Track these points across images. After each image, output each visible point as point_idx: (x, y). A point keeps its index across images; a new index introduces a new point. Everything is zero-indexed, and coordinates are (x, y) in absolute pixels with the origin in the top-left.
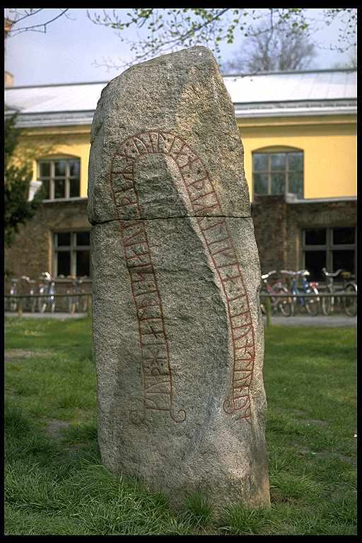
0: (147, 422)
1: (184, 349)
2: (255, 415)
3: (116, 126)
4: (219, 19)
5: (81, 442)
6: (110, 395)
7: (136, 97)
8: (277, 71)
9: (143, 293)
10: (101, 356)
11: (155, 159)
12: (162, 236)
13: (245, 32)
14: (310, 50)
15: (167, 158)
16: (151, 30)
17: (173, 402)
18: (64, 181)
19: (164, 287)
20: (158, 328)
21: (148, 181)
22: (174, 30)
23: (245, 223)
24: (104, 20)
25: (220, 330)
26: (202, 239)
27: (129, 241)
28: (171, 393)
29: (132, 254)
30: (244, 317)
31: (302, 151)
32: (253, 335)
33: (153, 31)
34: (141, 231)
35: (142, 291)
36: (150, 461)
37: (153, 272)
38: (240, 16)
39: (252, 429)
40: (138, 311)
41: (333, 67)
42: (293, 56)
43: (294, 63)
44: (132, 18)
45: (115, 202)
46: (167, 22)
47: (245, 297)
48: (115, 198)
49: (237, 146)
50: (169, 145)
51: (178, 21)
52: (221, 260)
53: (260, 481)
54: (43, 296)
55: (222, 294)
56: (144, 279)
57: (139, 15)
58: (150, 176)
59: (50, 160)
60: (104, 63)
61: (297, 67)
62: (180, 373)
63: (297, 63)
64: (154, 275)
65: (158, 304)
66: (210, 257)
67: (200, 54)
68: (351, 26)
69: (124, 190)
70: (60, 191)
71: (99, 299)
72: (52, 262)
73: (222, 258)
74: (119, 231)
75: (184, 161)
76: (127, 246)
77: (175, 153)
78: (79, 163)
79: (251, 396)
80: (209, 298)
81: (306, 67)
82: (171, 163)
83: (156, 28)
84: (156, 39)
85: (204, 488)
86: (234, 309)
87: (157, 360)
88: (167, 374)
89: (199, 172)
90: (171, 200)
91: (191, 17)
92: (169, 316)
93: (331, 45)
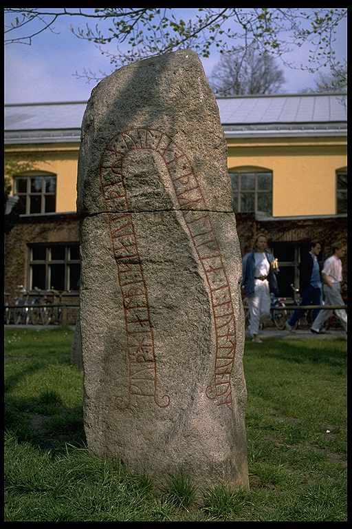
0: (132, 407)
2: (235, 401)
4: (196, 37)
5: (63, 434)
6: (96, 381)
8: (246, 95)
9: (129, 283)
10: (88, 343)
13: (220, 48)
14: (279, 76)
16: (131, 45)
17: (157, 388)
22: (153, 45)
23: (227, 218)
24: (87, 35)
26: (187, 231)
28: (156, 379)
30: (226, 306)
31: (271, 171)
33: (134, 45)
35: (129, 281)
36: (135, 445)
37: (140, 262)
38: (216, 35)
39: (233, 415)
41: (301, 93)
42: (262, 82)
43: (263, 88)
44: (113, 34)
46: (147, 38)
47: (227, 288)
48: (104, 192)
51: (157, 37)
52: (205, 252)
53: (240, 466)
54: (18, 307)
56: (130, 270)
57: (120, 31)
59: (27, 176)
60: (85, 75)
61: (267, 93)
63: (267, 88)
66: (194, 250)
67: (187, 57)
68: (321, 48)
69: (113, 184)
70: (36, 207)
71: (86, 289)
72: (29, 276)
73: (207, 250)
77: (162, 149)
78: (55, 180)
79: (232, 383)
80: (193, 288)
81: (275, 92)
83: (136, 43)
84: (136, 54)
85: (185, 471)
86: (217, 299)
87: (143, 347)
88: (152, 361)
89: (184, 168)
93: (302, 66)
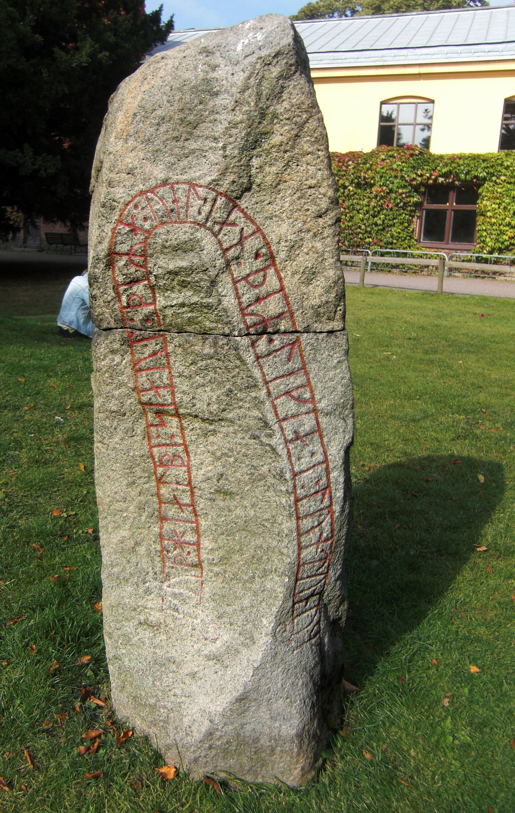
26: (257, 373)
56: (163, 424)
65: (184, 466)
89: (257, 255)
90: (208, 306)
91: (260, 52)
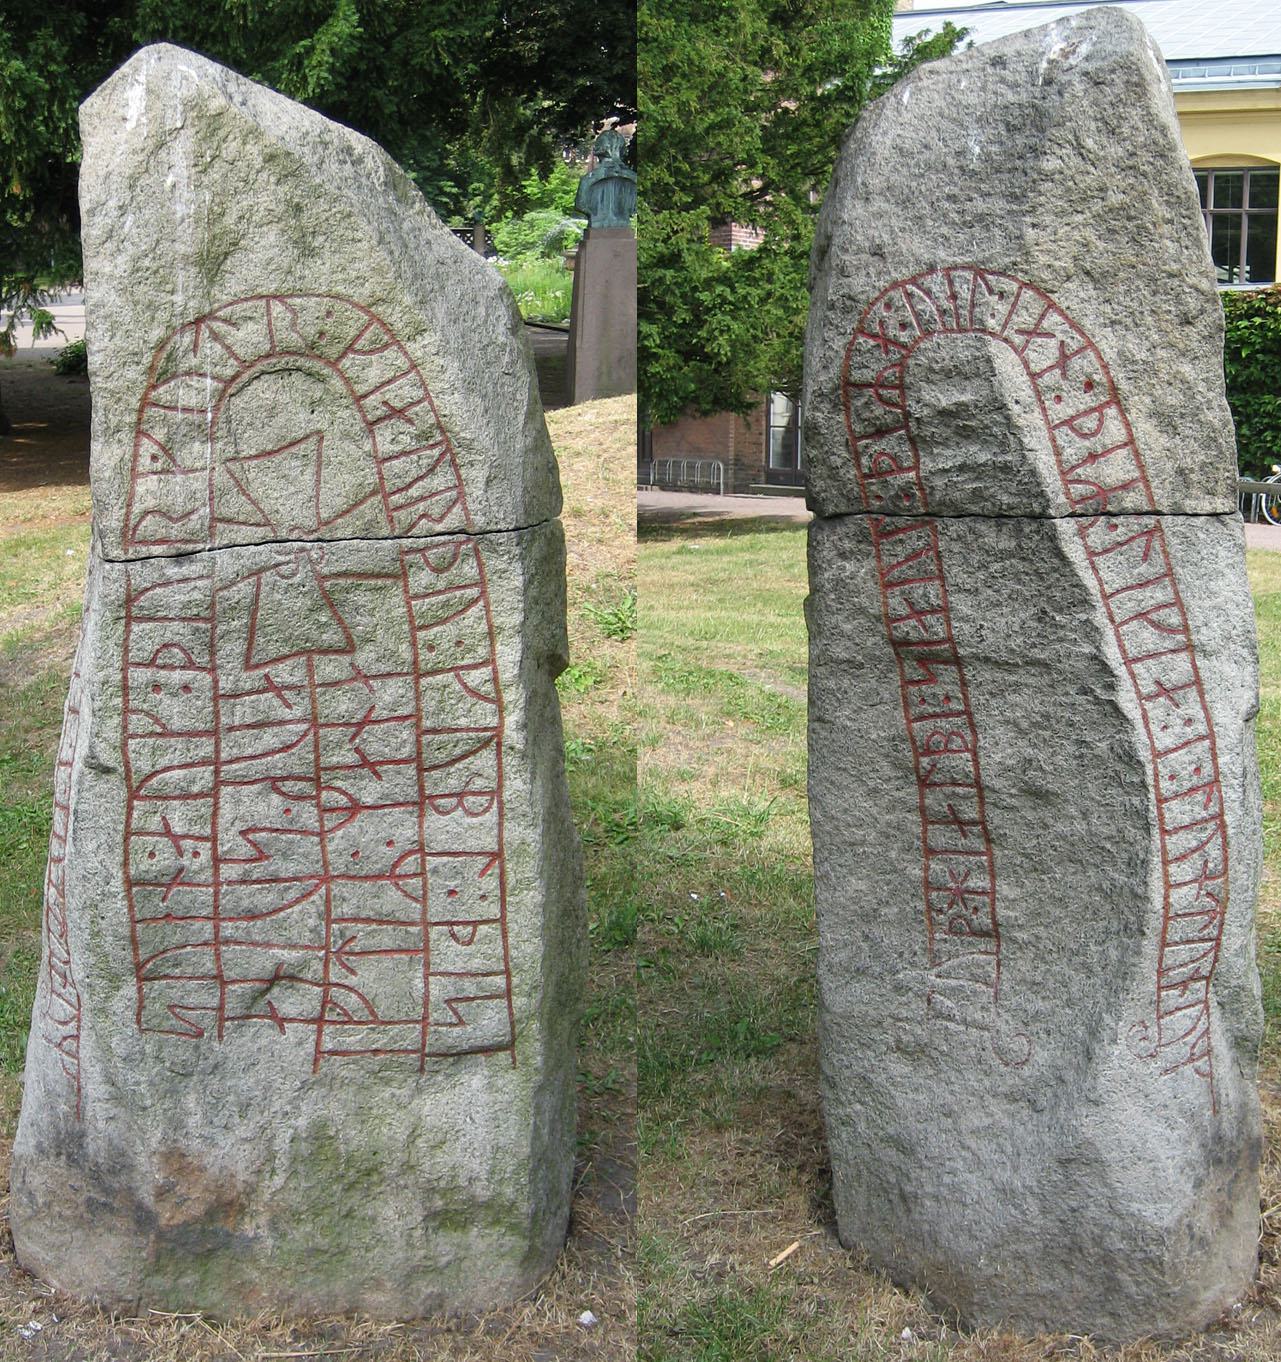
0: (935, 1054)
1: (1034, 875)
3: (860, 251)
7: (918, 165)
11: (958, 349)
12: (983, 566)
15: (995, 347)
18: (1239, 216)
19: (986, 706)
20: (970, 812)
21: (943, 413)
25: (1131, 833)
26: (1090, 581)
27: (896, 573)
29: (904, 610)
32: (1225, 845)
34: (929, 547)
37: (957, 661)
39: (1213, 1091)
40: (918, 762)
45: (859, 466)
47: (1207, 743)
48: (857, 456)
49: (1202, 311)
50: (1002, 308)
55: (1140, 735)
56: (931, 679)
58: (946, 397)
62: (1022, 936)
64: (960, 670)
65: (967, 750)
74: (871, 543)
75: (1043, 355)
76: (890, 585)
77: (1020, 332)
80: (1103, 745)
82: (1006, 362)
86: (1172, 778)
90: (1006, 468)
92: (997, 783)
